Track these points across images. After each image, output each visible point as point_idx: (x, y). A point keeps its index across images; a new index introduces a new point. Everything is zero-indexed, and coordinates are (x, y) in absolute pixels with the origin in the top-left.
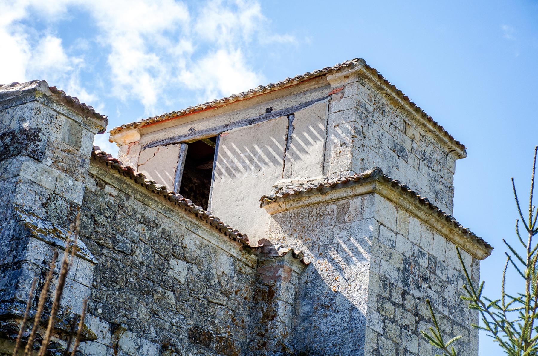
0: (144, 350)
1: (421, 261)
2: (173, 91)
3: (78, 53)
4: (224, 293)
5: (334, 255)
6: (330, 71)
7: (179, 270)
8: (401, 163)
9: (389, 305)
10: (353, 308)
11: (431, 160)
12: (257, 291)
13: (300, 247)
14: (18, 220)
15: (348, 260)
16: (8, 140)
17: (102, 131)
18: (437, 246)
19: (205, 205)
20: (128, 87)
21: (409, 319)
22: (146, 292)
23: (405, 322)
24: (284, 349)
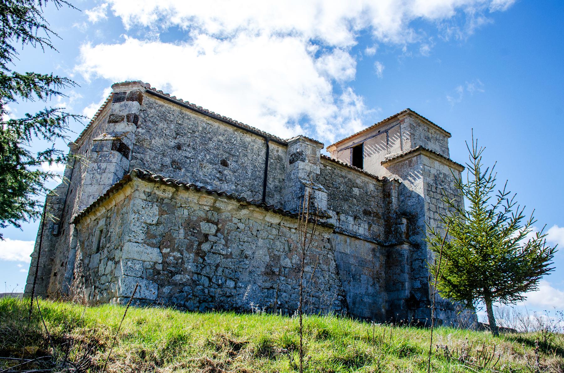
0: (349, 219)
1: (440, 176)
2: (338, 136)
3: (306, 129)
4: (373, 197)
5: (410, 178)
6: (398, 114)
7: (356, 191)
8: (429, 143)
9: (431, 193)
10: (419, 196)
11: (439, 140)
12: (384, 195)
13: (397, 177)
14: (301, 182)
15: (415, 179)
16: (293, 156)
17: (323, 148)
18: (445, 169)
19: (362, 168)
20: (323, 137)
21: (439, 196)
22: (346, 200)
23: (438, 198)
24: (396, 213)
